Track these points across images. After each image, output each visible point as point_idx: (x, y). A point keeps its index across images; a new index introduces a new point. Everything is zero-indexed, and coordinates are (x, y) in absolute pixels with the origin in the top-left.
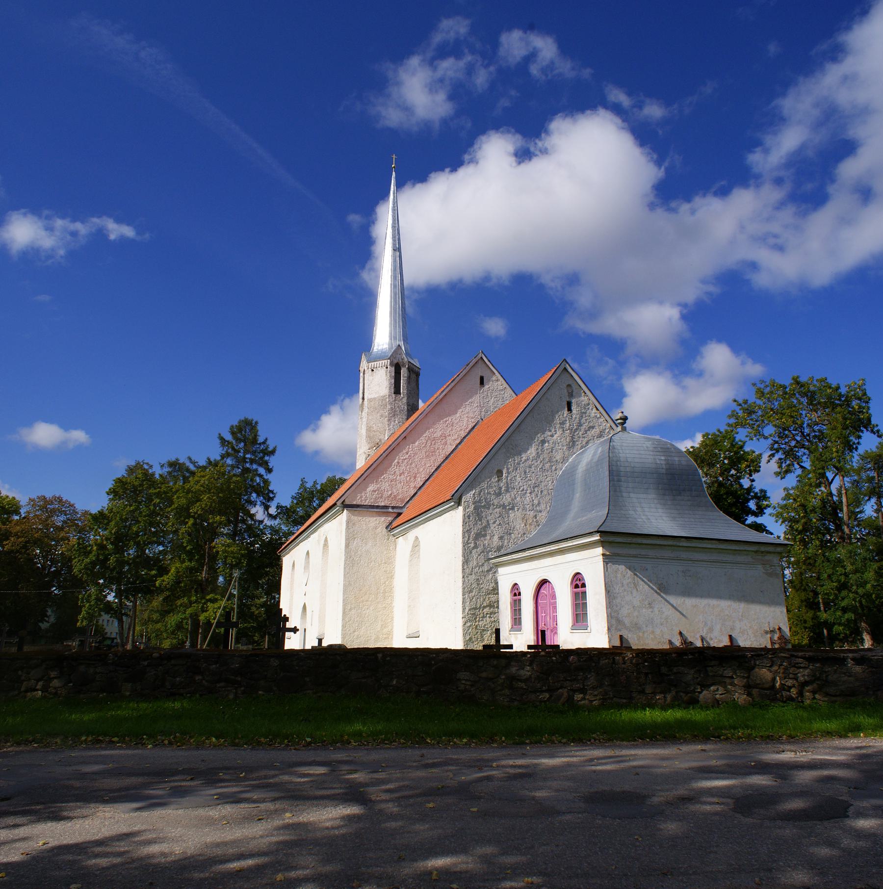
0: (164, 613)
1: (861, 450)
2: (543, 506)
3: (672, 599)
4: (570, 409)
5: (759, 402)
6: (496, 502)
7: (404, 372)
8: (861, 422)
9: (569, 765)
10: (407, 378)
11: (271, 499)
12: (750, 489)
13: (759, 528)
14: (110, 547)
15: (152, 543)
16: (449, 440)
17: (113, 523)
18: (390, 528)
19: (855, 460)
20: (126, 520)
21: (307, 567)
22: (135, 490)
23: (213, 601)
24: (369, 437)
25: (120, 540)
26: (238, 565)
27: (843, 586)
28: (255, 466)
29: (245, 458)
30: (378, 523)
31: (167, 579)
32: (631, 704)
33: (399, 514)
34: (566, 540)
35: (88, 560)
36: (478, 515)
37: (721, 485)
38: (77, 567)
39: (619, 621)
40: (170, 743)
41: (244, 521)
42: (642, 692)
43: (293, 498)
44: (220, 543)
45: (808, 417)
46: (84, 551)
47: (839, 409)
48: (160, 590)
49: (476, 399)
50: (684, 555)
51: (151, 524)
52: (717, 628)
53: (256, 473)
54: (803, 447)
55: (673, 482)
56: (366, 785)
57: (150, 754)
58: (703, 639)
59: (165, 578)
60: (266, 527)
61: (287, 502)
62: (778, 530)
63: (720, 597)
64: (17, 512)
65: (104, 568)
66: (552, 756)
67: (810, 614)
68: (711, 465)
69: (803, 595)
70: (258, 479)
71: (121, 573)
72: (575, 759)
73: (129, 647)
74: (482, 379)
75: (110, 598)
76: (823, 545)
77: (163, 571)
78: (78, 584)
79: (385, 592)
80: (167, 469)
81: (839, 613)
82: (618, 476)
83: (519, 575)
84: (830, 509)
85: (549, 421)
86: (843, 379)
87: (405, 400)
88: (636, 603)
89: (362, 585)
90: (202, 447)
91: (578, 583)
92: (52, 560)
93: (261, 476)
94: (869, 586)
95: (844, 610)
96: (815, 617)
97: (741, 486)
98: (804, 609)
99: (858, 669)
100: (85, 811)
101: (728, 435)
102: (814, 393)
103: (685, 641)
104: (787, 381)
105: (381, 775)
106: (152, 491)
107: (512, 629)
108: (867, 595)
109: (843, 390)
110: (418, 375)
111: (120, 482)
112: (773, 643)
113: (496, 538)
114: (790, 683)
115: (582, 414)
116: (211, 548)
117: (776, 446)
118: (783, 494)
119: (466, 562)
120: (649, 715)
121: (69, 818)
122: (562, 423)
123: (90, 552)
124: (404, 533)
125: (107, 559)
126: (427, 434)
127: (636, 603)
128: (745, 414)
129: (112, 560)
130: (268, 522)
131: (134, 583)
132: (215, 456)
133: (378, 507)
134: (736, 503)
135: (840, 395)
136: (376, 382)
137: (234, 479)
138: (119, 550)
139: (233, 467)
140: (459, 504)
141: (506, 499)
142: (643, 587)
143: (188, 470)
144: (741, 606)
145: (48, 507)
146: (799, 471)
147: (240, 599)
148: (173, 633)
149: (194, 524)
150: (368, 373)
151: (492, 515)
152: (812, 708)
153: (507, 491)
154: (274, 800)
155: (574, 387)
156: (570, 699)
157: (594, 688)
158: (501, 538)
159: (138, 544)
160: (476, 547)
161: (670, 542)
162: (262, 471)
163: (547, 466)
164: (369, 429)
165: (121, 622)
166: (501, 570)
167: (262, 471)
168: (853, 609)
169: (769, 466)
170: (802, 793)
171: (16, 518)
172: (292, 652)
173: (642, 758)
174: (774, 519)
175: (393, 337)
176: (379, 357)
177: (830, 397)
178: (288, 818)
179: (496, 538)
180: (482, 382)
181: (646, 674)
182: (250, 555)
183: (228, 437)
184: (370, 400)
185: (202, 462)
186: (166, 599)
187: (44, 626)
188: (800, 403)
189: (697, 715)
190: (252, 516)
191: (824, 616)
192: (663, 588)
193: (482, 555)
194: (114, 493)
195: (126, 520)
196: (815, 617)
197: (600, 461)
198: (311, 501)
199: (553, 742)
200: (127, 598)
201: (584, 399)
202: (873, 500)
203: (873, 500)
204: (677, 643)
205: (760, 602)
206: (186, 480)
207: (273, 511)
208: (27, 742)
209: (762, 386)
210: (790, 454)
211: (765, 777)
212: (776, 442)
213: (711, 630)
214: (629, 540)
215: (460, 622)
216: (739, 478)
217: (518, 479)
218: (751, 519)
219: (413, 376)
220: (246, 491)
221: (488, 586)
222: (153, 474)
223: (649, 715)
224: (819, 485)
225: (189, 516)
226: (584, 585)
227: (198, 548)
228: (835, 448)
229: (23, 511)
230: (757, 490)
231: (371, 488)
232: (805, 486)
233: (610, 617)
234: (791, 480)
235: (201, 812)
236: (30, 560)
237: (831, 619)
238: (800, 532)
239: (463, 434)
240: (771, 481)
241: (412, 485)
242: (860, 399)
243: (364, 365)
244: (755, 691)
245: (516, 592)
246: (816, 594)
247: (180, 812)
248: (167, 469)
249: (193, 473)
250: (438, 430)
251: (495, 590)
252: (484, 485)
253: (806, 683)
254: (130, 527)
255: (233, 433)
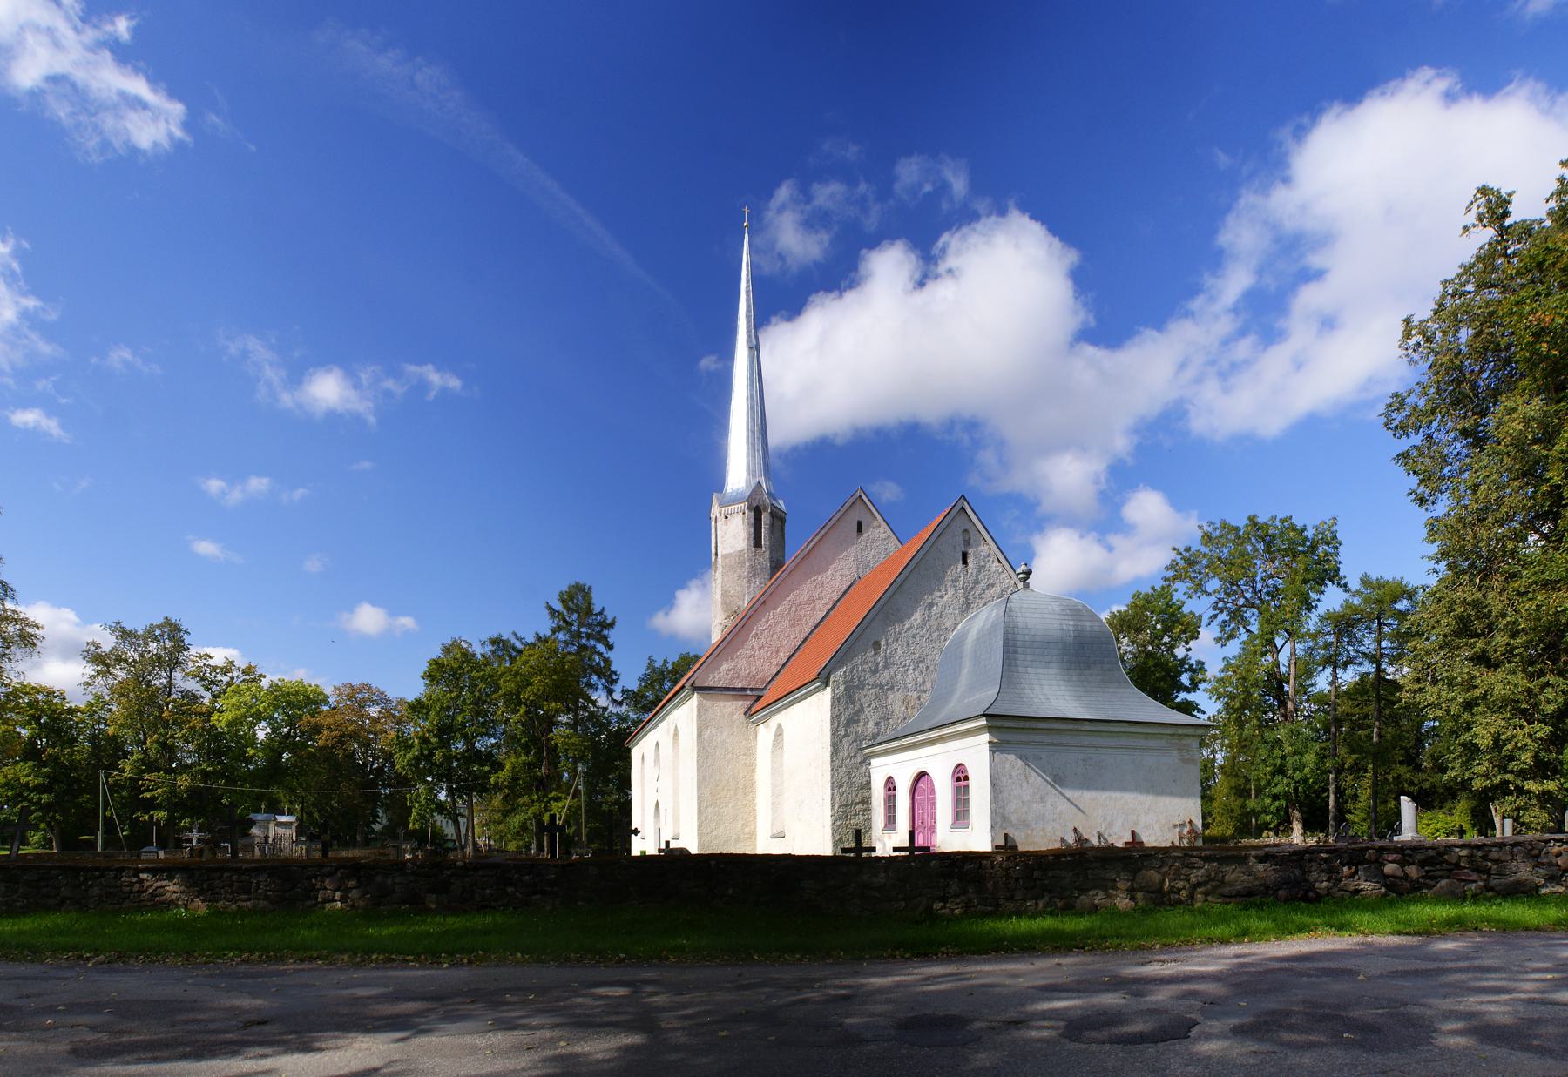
0: (506, 813)
1: (1322, 609)
2: (928, 686)
3: (1069, 793)
4: (965, 562)
5: (1205, 550)
6: (871, 681)
7: (765, 517)
8: (1328, 574)
9: (899, 985)
10: (768, 523)
11: (616, 681)
12: (1183, 661)
13: (1188, 708)
14: (434, 740)
15: (482, 735)
16: (819, 604)
17: (432, 713)
18: (749, 713)
19: (1312, 622)
20: (448, 708)
21: (657, 759)
22: (454, 672)
23: (557, 799)
24: (724, 603)
25: (445, 732)
26: (581, 759)
27: (1281, 771)
28: (592, 642)
29: (579, 633)
30: (732, 708)
31: (503, 776)
32: (997, 913)
33: (760, 697)
34: (947, 725)
35: (409, 756)
36: (850, 697)
37: (1149, 655)
38: (401, 763)
39: (1004, 818)
40: (470, 962)
41: (585, 708)
42: (1011, 898)
43: (641, 680)
44: (559, 734)
45: (1262, 568)
46: (404, 744)
47: (1301, 557)
48: (498, 787)
49: (853, 551)
50: (1086, 740)
51: (478, 713)
52: (1119, 822)
53: (594, 651)
54: (1253, 606)
55: (1081, 653)
56: (664, 1009)
57: (445, 975)
58: (1100, 836)
59: (501, 774)
60: (611, 714)
61: (634, 686)
62: (1209, 706)
63: (1124, 789)
64: (326, 702)
65: (424, 763)
66: (884, 974)
67: (1239, 802)
68: (1138, 630)
69: (1233, 782)
70: (597, 658)
71: (450, 768)
72: (909, 978)
73: (469, 849)
74: (860, 524)
75: (442, 796)
76: (1264, 726)
77: (498, 766)
78: (403, 782)
79: (745, 787)
80: (489, 648)
81: (1269, 801)
82: (1014, 648)
83: (893, 768)
84: (1275, 683)
85: (939, 579)
86: (1309, 519)
87: (767, 555)
88: (1027, 797)
89: (720, 782)
90: (529, 622)
91: (960, 775)
92: (373, 756)
93: (600, 654)
94: (1307, 770)
95: (1275, 797)
96: (1243, 806)
97: (1175, 657)
98: (1232, 798)
99: (1260, 867)
100: (340, 1042)
101: (1165, 593)
102: (1273, 536)
103: (1080, 839)
104: (1241, 522)
105: (686, 998)
106: (474, 674)
107: (886, 828)
108: (1305, 780)
109: (1309, 533)
110: (783, 521)
111: (437, 664)
112: (1181, 838)
113: (871, 724)
114: (1180, 884)
115: (980, 568)
116: (548, 740)
117: (1221, 605)
118: (1222, 665)
119: (835, 752)
120: (1023, 925)
121: (320, 1050)
122: (955, 581)
123: (412, 746)
124: (765, 719)
125: (431, 754)
126: (791, 597)
127: (1027, 797)
128: (1187, 566)
129: (438, 755)
130: (613, 709)
131: (465, 780)
132: (545, 631)
133: (734, 689)
134: (1160, 678)
135: (1306, 539)
136: (731, 533)
137: (569, 658)
138: (445, 744)
139: (567, 643)
140: (827, 685)
141: (884, 677)
142: (1036, 779)
143: (514, 648)
144: (1148, 799)
145: (359, 697)
146: (1244, 637)
147: (589, 794)
148: (518, 833)
149: (527, 712)
150: (721, 520)
151: (867, 696)
152: (1201, 912)
153: (885, 667)
154: (553, 1027)
155: (972, 532)
156: (929, 908)
157: (957, 896)
158: (877, 724)
159: (465, 736)
160: (847, 735)
161: (1070, 726)
162: (601, 647)
163: (935, 635)
164: (725, 594)
165: (456, 823)
166: (874, 762)
167: (601, 647)
168: (1286, 795)
169: (1207, 634)
170: (1153, 1012)
171: (325, 708)
172: (644, 857)
173: (988, 974)
174: (1207, 695)
175: (751, 472)
176: (735, 500)
177: (1292, 542)
178: (563, 1048)
179: (871, 724)
180: (860, 530)
181: (1017, 880)
182: (595, 746)
183: (558, 606)
184: (725, 557)
185: (530, 639)
186: (505, 798)
187: (377, 827)
188: (1256, 550)
189: (1070, 924)
190: (594, 703)
191: (1252, 804)
192: (1059, 780)
193: (852, 746)
194: (429, 676)
195: (448, 708)
196: (1243, 806)
197: (993, 627)
198: (662, 684)
199: (894, 957)
200: (460, 797)
201: (983, 549)
202: (1329, 670)
203: (1329, 670)
204: (1071, 839)
205: (1171, 794)
206: (512, 660)
207: (617, 696)
208: (312, 959)
209: (1210, 529)
210: (1237, 615)
211: (1116, 995)
212: (1221, 600)
213: (1111, 825)
214: (1022, 724)
215: (829, 821)
216: (1173, 647)
217: (900, 652)
218: (1182, 696)
219: (778, 523)
220: (584, 671)
221: (858, 780)
222: (474, 655)
223: (1023, 925)
224: (1264, 654)
225: (520, 703)
226: (966, 778)
227: (535, 740)
228: (1290, 605)
229: (331, 700)
230: (1192, 661)
231: (725, 666)
232: (1250, 655)
233: (994, 813)
234: (1234, 648)
235: (468, 1039)
236: (351, 756)
237: (1259, 808)
238: (1236, 711)
239: (835, 597)
240: (1209, 650)
241: (774, 661)
242: (1328, 544)
243: (715, 510)
244: (1139, 895)
245: (890, 785)
246: (1248, 780)
247: (445, 1039)
248: (489, 648)
249: (520, 652)
250: (804, 592)
251: (868, 784)
252: (858, 660)
253: (1199, 884)
254: (453, 718)
255: (563, 601)
